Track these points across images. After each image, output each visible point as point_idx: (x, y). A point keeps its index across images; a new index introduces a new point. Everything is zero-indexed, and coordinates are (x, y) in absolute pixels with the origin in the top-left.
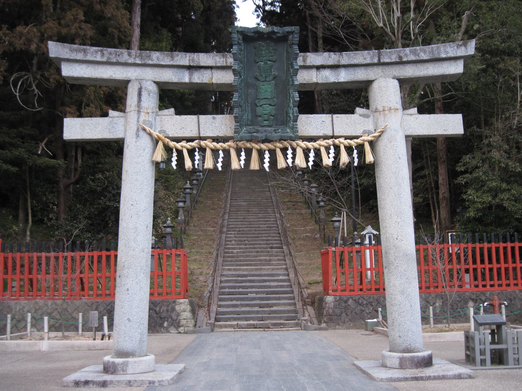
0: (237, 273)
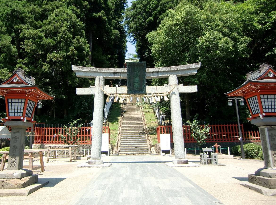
0: (127, 135)
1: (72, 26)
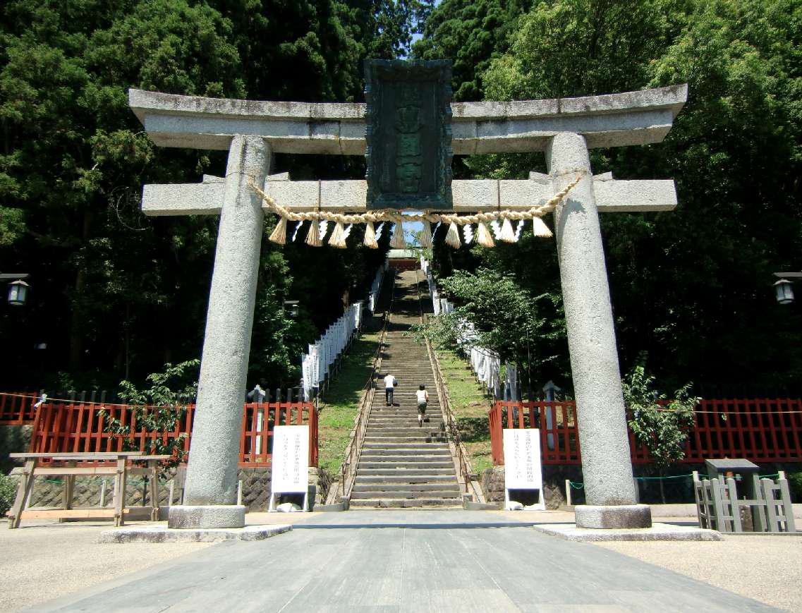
1: (196, 54)
